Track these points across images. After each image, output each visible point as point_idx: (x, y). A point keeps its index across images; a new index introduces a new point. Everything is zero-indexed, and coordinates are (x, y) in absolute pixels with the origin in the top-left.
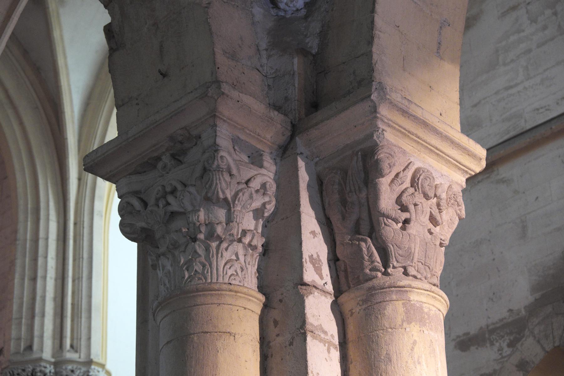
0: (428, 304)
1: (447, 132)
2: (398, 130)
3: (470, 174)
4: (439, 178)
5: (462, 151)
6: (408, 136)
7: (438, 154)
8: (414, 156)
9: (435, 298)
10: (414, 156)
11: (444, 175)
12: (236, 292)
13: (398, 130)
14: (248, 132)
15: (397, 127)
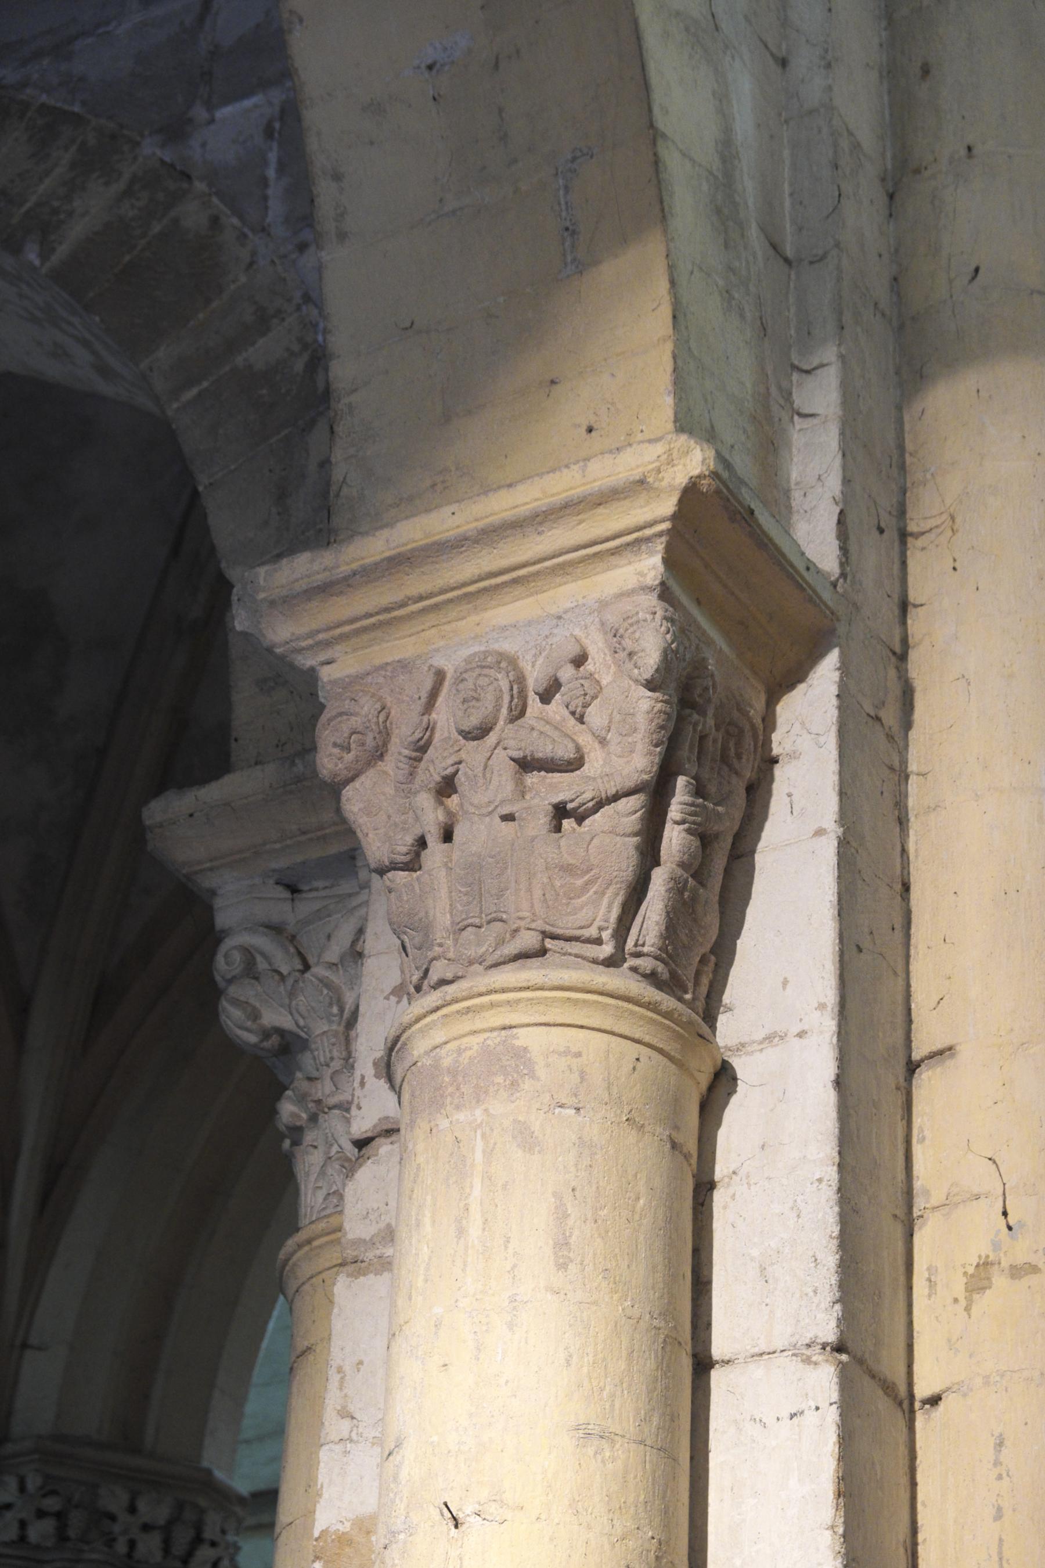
0: (455, 1039)
1: (487, 517)
2: (358, 632)
3: (660, 534)
4: (555, 631)
5: (569, 515)
6: (395, 618)
7: (515, 581)
8: (437, 650)
9: (468, 1010)
10: (437, 650)
11: (565, 612)
12: (309, 1242)
13: (358, 632)
14: (278, 846)
15: (347, 629)
